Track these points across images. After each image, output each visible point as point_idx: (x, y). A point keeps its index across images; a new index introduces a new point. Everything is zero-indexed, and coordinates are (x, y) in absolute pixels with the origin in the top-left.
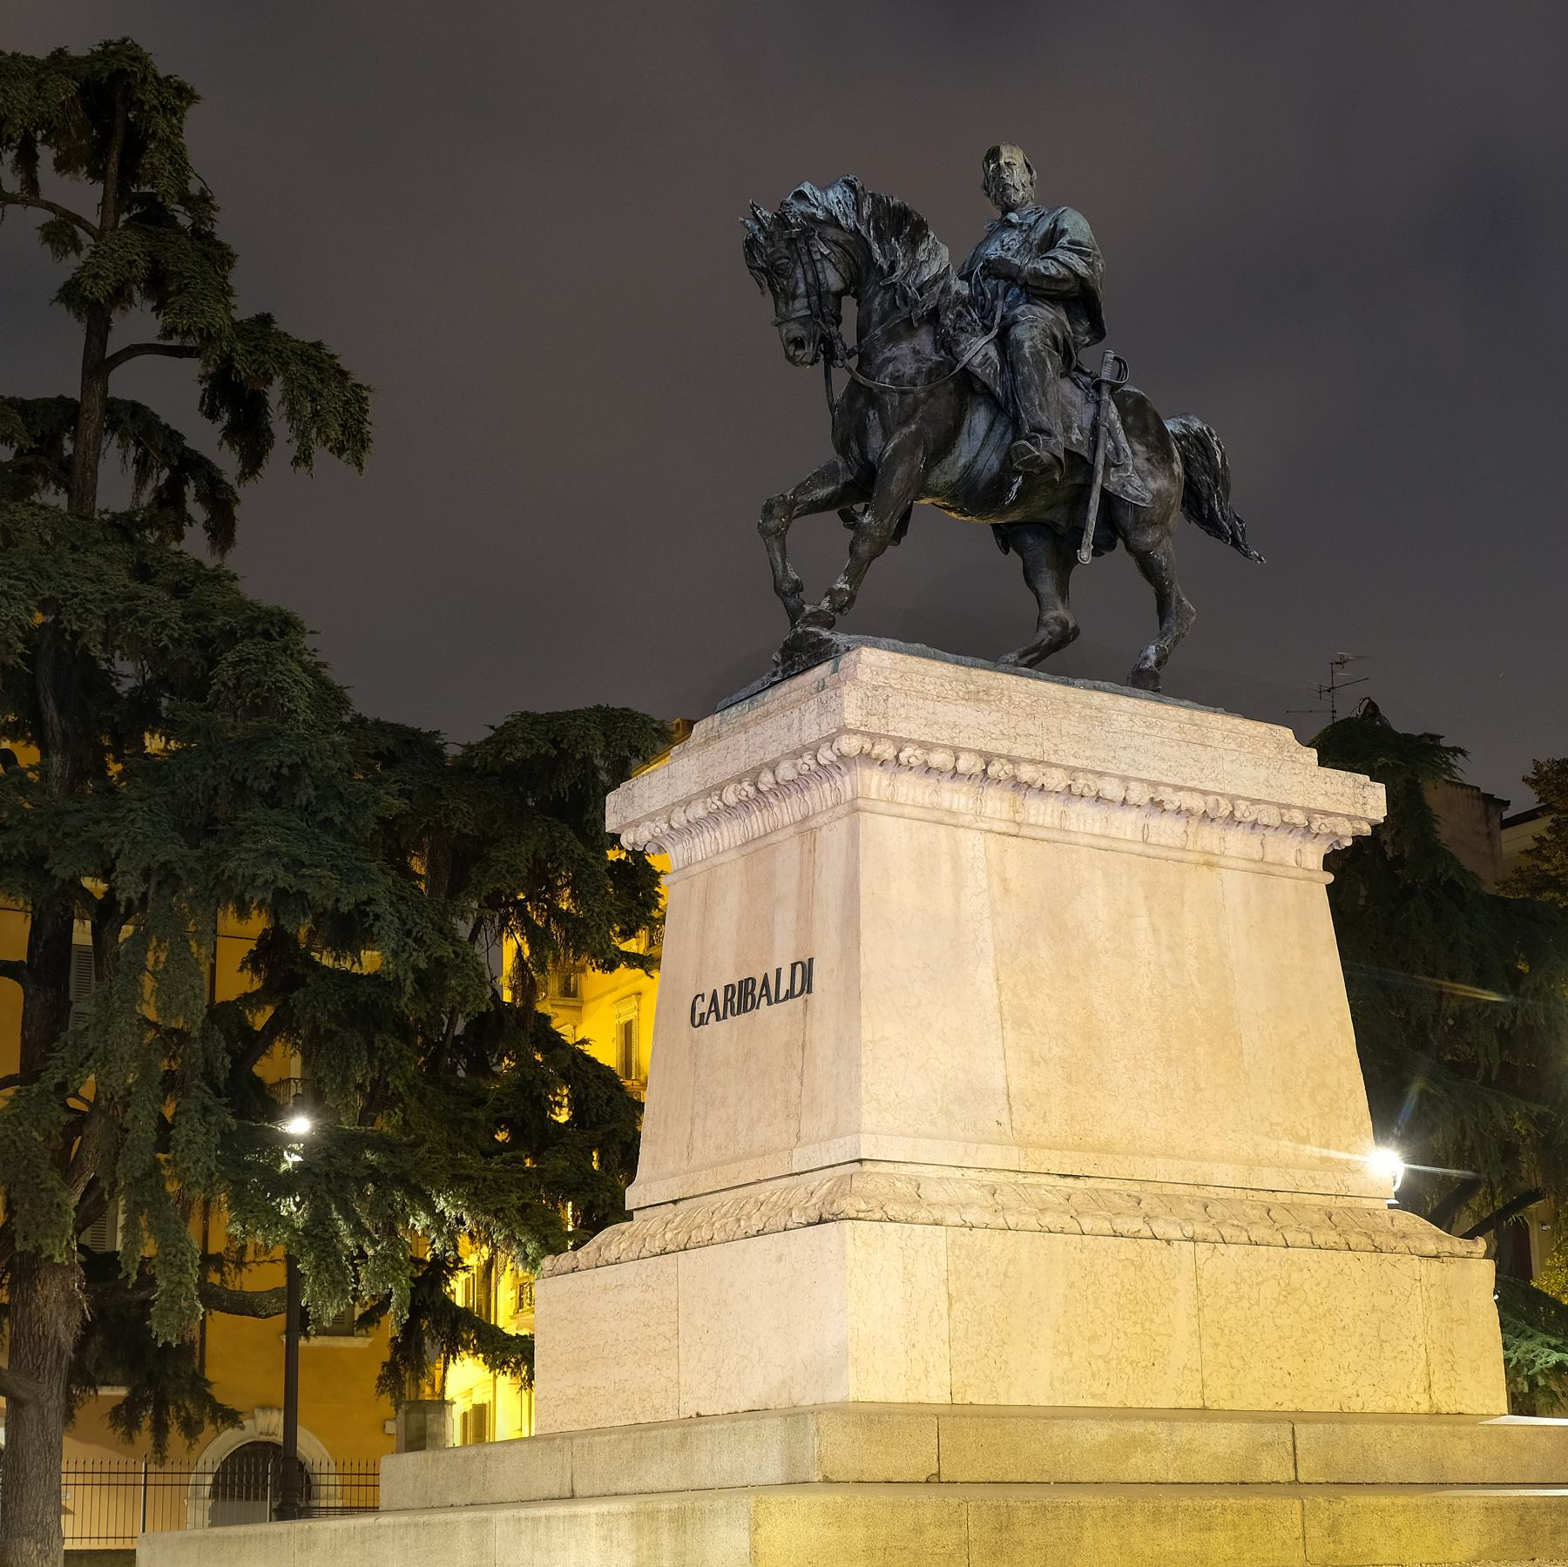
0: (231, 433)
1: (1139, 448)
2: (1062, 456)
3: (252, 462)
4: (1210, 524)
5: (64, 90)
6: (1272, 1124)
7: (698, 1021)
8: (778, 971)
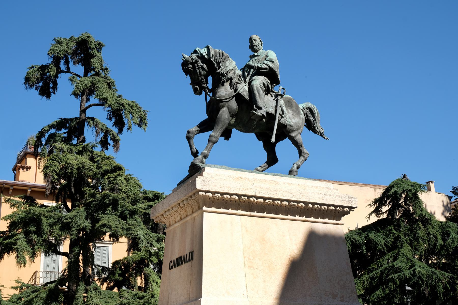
0: (115, 124)
1: (290, 111)
2: (265, 115)
3: (120, 131)
4: (314, 131)
6: (326, 291)
7: (171, 268)
8: (187, 254)
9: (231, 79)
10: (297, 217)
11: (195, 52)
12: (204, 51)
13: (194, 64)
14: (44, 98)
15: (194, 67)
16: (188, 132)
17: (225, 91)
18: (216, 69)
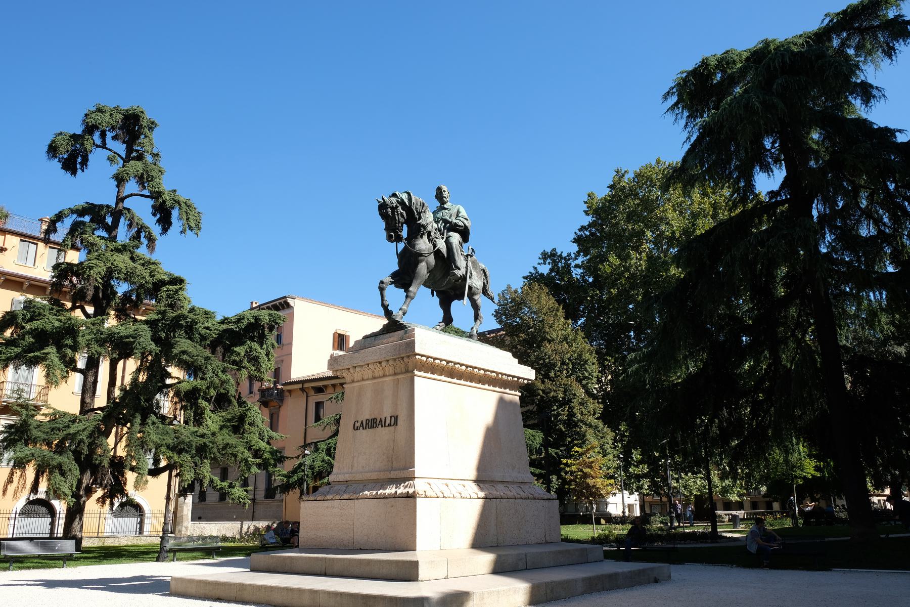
0: (159, 221)
3: (165, 230)
5: (119, 117)
7: (356, 429)
9: (429, 233)
10: (486, 386)
11: (394, 195)
12: (405, 197)
13: (394, 209)
14: (69, 174)
15: (393, 212)
16: (382, 282)
17: (423, 244)
18: (416, 220)
